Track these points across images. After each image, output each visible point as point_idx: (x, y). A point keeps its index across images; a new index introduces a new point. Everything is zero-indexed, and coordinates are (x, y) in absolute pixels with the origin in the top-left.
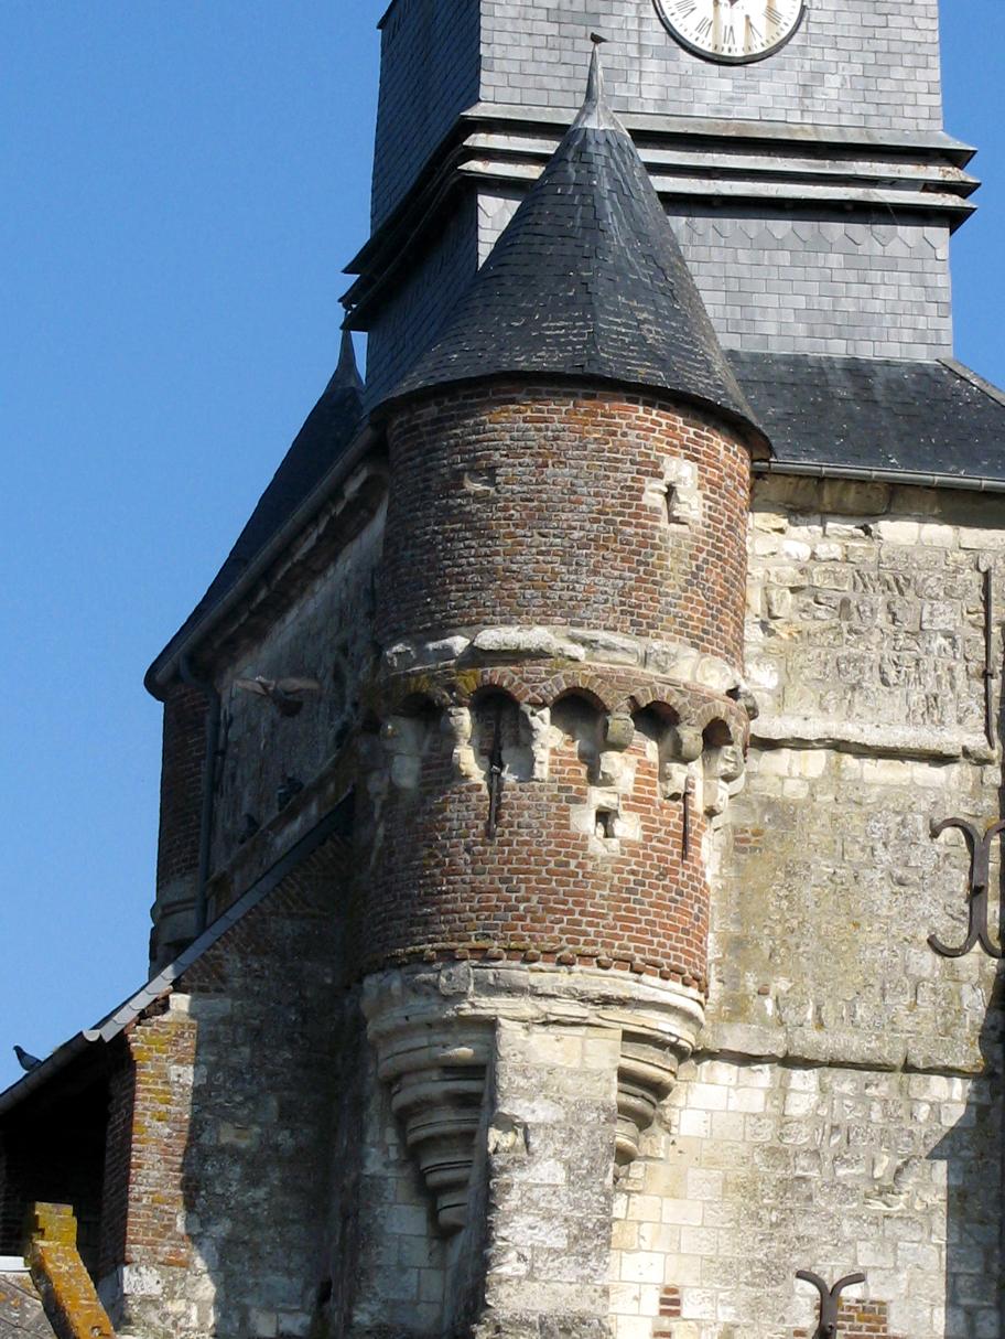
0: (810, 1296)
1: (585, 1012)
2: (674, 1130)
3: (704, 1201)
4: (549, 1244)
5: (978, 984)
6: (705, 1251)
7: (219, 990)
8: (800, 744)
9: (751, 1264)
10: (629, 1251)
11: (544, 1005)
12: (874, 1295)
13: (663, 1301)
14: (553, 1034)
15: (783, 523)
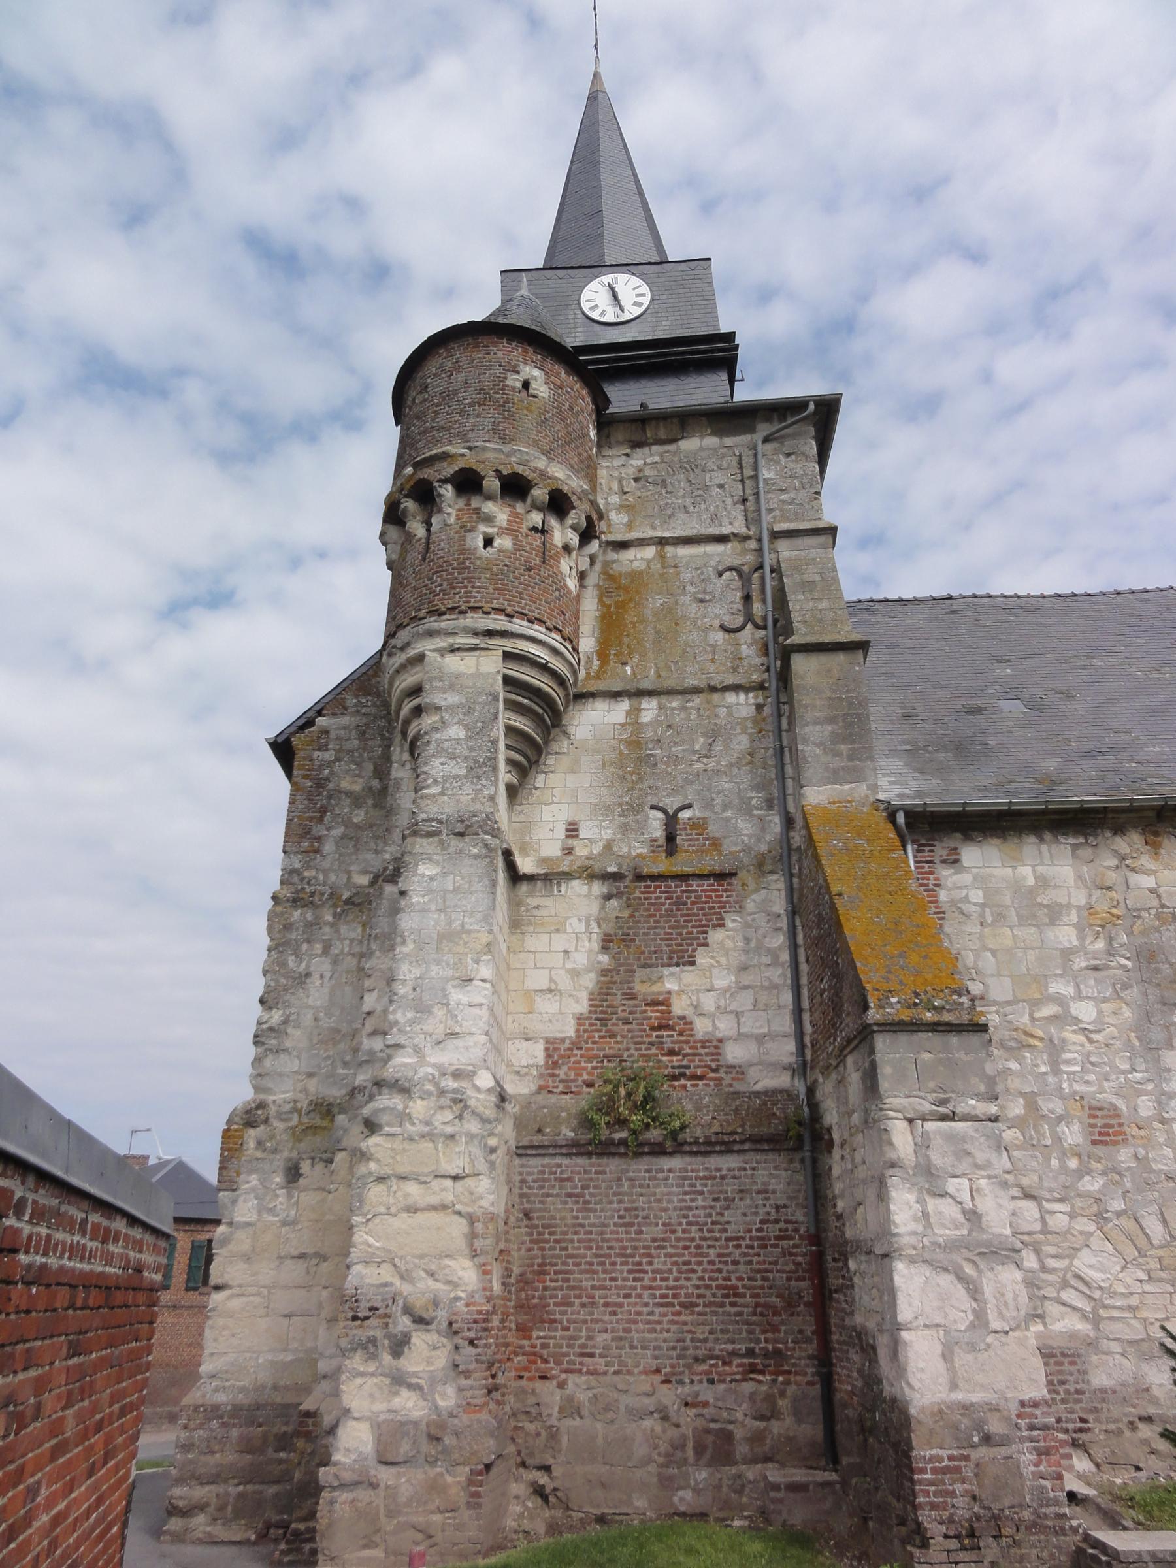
1: (476, 641)
4: (454, 772)
5: (752, 644)
7: (343, 714)
8: (642, 543)
9: (621, 805)
11: (451, 640)
12: (698, 815)
13: (567, 830)
15: (628, 451)
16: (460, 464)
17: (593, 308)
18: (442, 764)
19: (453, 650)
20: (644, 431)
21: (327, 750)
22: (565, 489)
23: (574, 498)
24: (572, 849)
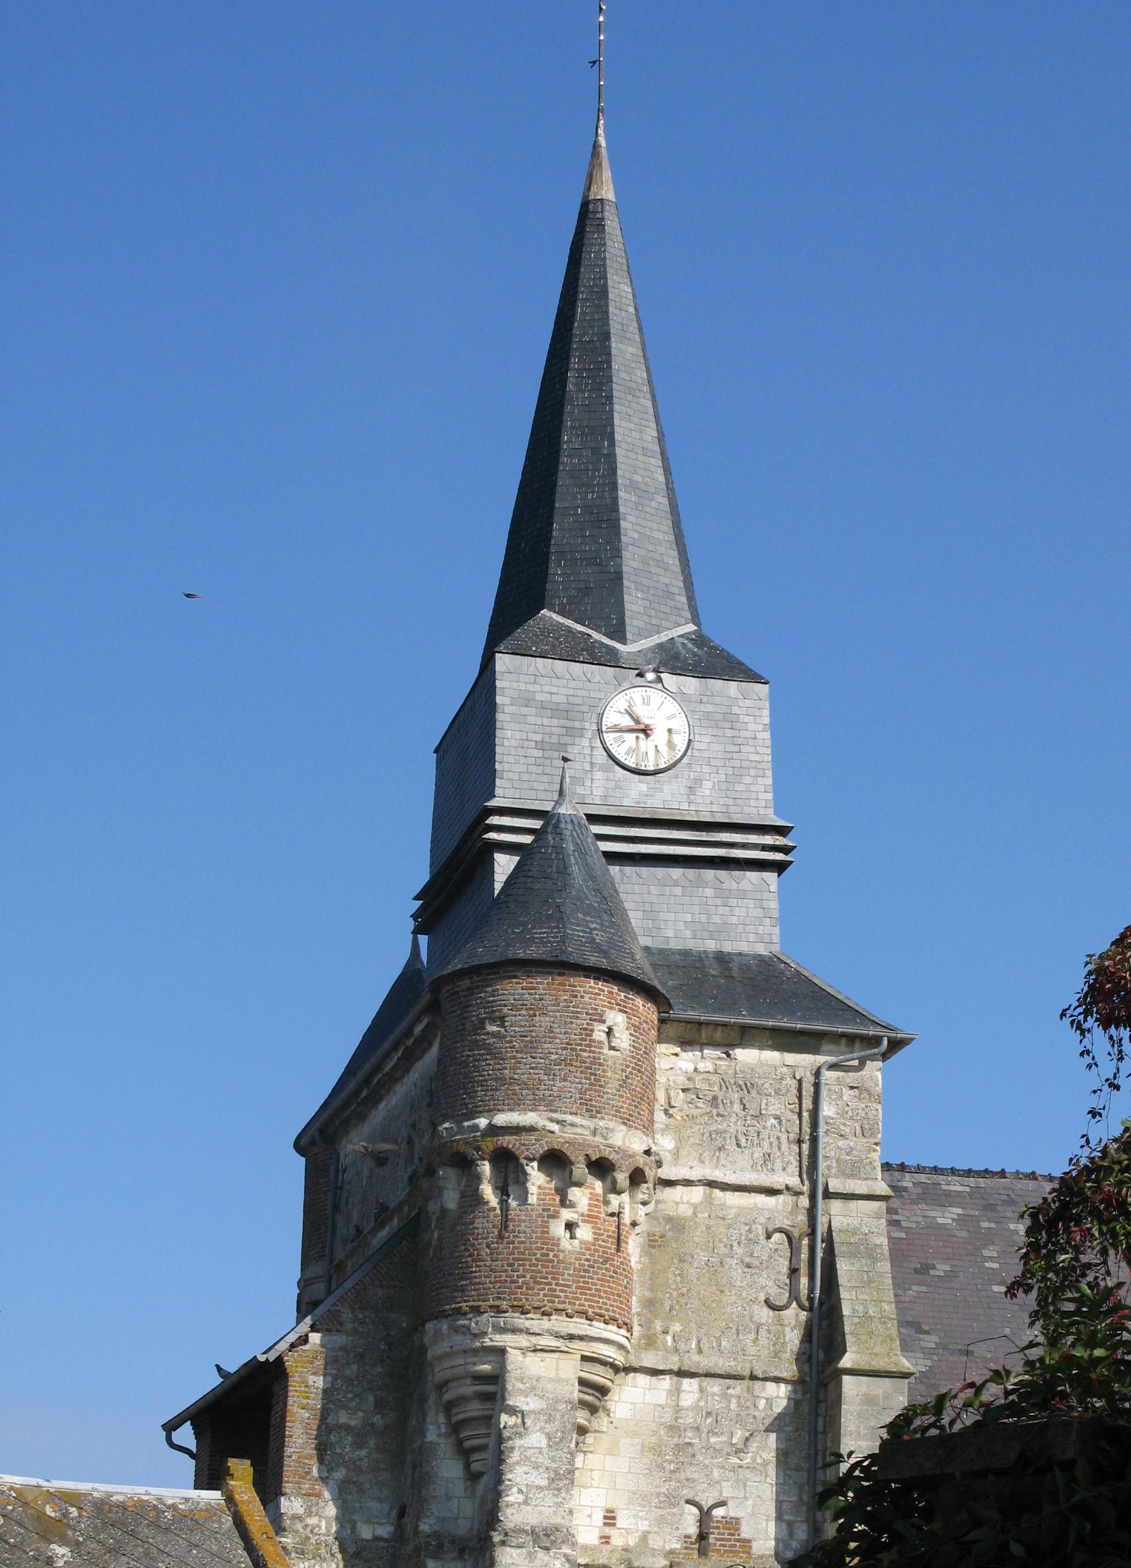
1: (558, 1344)
2: (612, 1415)
3: (630, 1458)
5: (795, 1327)
6: (630, 1488)
9: (658, 1495)
11: (534, 1339)
12: (732, 1514)
13: (605, 1518)
15: (678, 1050)
24: (608, 1537)
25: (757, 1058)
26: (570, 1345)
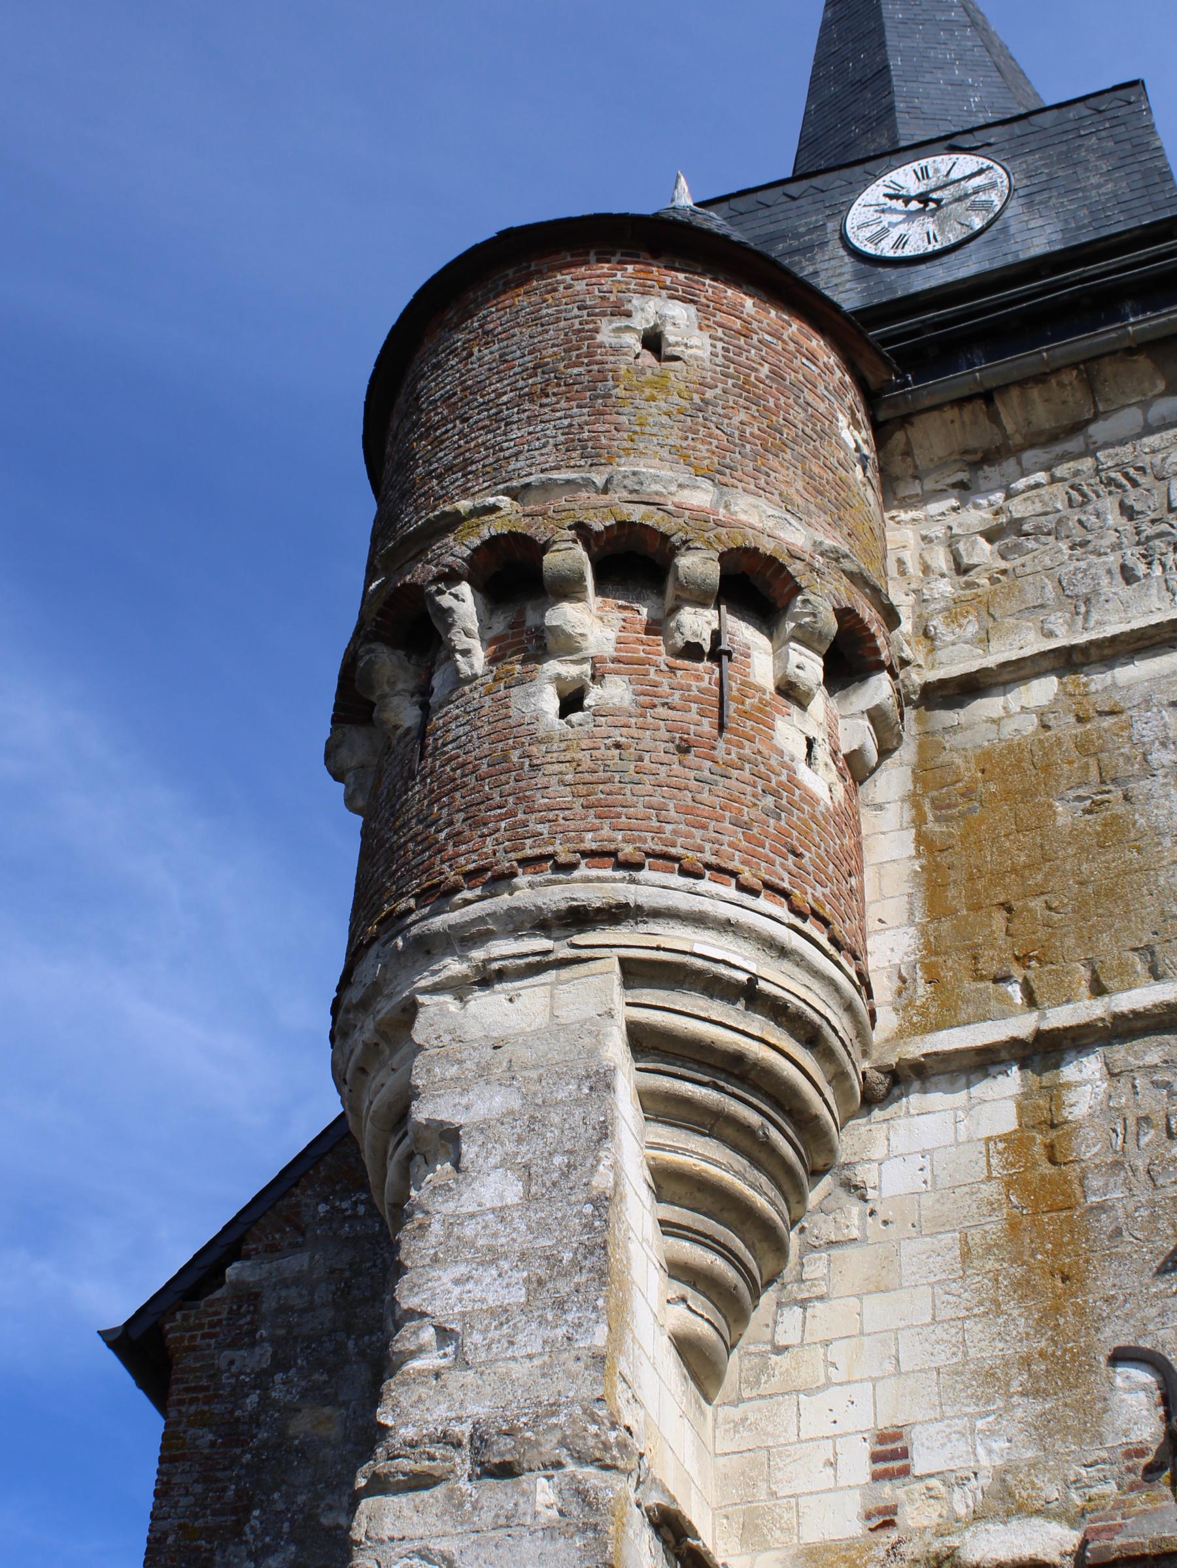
0: (1144, 1388)
2: (871, 1194)
3: (932, 1285)
6: (941, 1360)
10: (809, 1392)
13: (876, 1458)
14: (504, 991)
16: (491, 527)
17: (875, 239)
18: (457, 1282)
19: (487, 978)
20: (995, 418)
21: (253, 1344)
22: (767, 547)
23: (795, 567)
24: (893, 1510)
25: (1141, 423)
26: (579, 939)
